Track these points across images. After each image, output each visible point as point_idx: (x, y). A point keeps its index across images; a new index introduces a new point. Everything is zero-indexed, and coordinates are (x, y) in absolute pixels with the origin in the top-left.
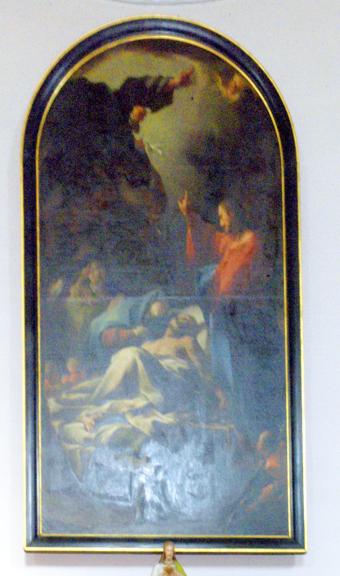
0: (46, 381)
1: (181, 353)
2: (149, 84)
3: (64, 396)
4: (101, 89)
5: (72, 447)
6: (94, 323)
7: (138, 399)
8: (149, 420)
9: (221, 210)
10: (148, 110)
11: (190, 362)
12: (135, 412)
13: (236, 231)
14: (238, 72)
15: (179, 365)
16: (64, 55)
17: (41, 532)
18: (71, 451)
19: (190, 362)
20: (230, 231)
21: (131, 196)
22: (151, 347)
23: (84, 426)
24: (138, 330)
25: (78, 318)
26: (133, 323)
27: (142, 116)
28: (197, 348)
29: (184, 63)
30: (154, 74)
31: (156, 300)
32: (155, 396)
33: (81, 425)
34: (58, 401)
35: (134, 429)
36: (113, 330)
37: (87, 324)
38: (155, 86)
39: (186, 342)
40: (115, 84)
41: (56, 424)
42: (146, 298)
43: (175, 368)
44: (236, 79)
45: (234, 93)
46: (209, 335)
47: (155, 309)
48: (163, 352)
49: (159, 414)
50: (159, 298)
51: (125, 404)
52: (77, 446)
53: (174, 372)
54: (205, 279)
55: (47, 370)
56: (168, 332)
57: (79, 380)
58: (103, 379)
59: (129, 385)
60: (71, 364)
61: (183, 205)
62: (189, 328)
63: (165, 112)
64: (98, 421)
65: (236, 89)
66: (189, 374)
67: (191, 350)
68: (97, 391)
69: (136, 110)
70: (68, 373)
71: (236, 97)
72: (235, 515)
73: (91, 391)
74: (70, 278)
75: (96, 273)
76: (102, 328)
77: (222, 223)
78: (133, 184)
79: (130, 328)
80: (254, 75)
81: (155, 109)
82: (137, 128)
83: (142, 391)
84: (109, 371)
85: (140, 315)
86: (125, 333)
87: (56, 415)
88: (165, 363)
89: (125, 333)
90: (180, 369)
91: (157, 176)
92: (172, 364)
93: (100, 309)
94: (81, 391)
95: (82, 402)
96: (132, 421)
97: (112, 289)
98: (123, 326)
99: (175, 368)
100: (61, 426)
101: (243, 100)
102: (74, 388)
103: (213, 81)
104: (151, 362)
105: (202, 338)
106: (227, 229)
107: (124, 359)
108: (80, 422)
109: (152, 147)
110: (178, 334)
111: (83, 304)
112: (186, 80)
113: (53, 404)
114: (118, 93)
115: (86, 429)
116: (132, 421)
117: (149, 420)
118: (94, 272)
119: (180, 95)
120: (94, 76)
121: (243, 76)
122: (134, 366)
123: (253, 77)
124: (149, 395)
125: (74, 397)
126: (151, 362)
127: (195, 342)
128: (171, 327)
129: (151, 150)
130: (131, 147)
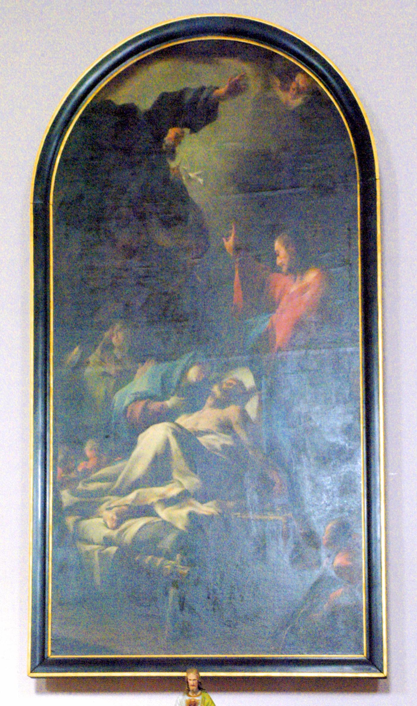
0: (59, 470)
1: (226, 427)
2: (188, 97)
3: (80, 486)
4: (128, 112)
5: (88, 548)
6: (116, 398)
7: (170, 486)
8: (184, 512)
9: (278, 246)
10: (187, 130)
11: (235, 437)
12: (167, 502)
13: (298, 268)
14: (300, 70)
15: (222, 442)
16: (274, 693)
17: (50, 653)
18: (87, 553)
19: (235, 437)
20: (290, 270)
21: (163, 238)
22: (186, 421)
23: (104, 521)
24: (171, 402)
25: (99, 391)
26: (165, 394)
27: (178, 139)
28: (244, 416)
29: (234, 67)
30: (195, 85)
31: (194, 364)
32: (191, 482)
33: (101, 520)
34: (74, 493)
35: (164, 522)
36: (142, 404)
37: (108, 399)
38: (194, 102)
39: (232, 412)
40: (145, 104)
41: (70, 520)
42: (181, 363)
43: (218, 445)
44: (299, 78)
45: (295, 97)
46: (260, 402)
47: (193, 374)
48: (201, 427)
49: (198, 504)
50: (198, 360)
51: (153, 494)
52: (95, 547)
53: (216, 450)
54: (255, 333)
55: (61, 457)
56: (210, 401)
57: (99, 467)
58: (128, 464)
59: (159, 470)
60: (89, 448)
61: (229, 243)
62: (236, 395)
63: (206, 131)
64: (122, 518)
65: (299, 91)
66: (234, 453)
67: (237, 423)
68: (120, 478)
69: (172, 132)
70: (83, 456)
71: (299, 101)
72: (292, 628)
73: (113, 478)
74: (89, 345)
75: (121, 335)
76: (127, 401)
77: (279, 261)
78: (167, 224)
79: (162, 399)
80: (284, 45)
81: (194, 129)
82: (172, 153)
83: (175, 475)
84: (135, 453)
85: (174, 382)
86: (155, 406)
87: (71, 510)
88: (204, 440)
89: (155, 406)
90: (224, 446)
91: (196, 207)
92: (215, 441)
93: (124, 377)
94: (102, 479)
95: (101, 493)
96: (163, 513)
97: (140, 355)
98: (153, 398)
99: (218, 445)
100: (77, 522)
101: (308, 104)
102: (94, 476)
103: (267, 86)
104: (185, 437)
105: (252, 407)
106: (284, 269)
107: (154, 438)
108: (99, 517)
109: (191, 175)
110: (221, 404)
111: (104, 374)
112: (236, 89)
113: (67, 497)
114: (149, 112)
115: (106, 524)
116: (163, 513)
117: (184, 512)
118: (118, 335)
119: (224, 108)
120: (121, 97)
121: (308, 76)
122: (167, 444)
123: (322, 77)
124: (185, 481)
125: (93, 487)
126: (185, 437)
127: (244, 414)
128: (213, 395)
129: (189, 178)
130: (166, 181)
